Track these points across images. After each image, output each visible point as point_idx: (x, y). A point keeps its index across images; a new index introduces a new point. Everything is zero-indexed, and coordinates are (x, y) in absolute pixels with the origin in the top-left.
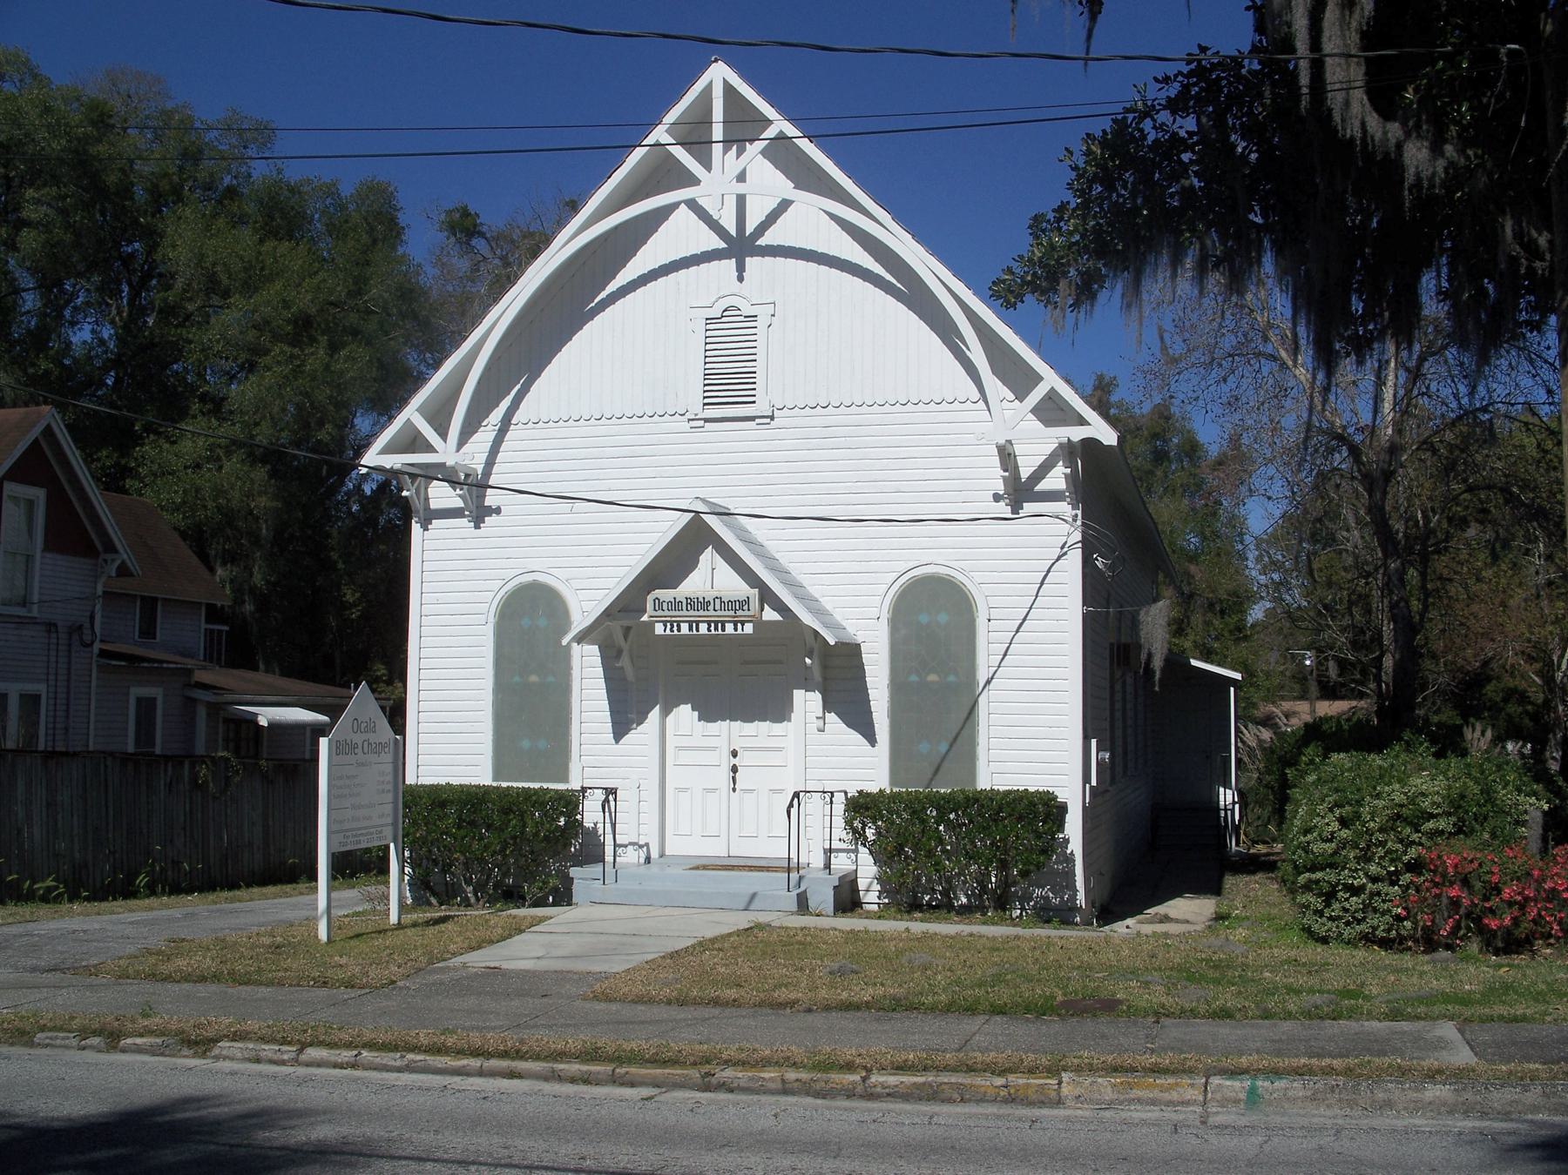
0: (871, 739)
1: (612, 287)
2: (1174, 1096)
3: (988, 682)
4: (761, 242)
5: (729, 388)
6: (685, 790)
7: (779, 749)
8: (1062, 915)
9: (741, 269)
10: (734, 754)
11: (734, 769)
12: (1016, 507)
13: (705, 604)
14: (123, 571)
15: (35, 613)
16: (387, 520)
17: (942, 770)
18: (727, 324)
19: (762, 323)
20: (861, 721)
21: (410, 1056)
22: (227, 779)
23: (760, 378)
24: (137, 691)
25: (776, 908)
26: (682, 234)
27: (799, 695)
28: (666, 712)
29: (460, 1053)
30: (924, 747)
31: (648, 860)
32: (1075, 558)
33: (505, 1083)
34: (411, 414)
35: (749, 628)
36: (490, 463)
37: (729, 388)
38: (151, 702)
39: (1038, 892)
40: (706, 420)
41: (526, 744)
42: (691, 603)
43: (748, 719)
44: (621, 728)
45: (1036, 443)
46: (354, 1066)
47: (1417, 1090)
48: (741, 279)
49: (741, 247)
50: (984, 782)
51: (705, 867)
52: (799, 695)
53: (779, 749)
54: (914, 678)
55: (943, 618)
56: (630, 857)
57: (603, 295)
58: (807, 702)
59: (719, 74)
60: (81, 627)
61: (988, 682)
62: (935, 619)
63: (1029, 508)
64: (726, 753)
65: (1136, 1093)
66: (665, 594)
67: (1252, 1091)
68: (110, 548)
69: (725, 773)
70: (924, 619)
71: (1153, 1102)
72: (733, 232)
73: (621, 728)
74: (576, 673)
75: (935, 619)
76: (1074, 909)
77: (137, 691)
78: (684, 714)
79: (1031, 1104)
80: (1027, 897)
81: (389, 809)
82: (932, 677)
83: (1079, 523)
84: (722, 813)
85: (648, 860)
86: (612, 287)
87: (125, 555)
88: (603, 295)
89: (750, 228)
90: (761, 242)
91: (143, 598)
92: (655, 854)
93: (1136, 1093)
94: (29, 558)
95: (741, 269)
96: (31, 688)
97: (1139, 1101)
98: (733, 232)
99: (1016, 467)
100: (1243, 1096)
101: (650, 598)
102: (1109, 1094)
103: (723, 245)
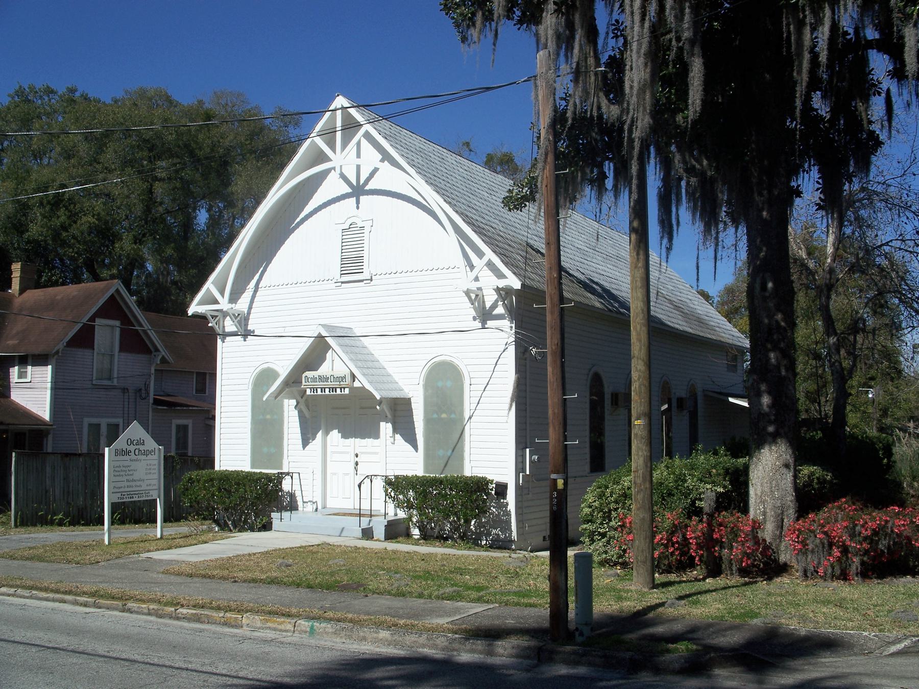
0: (416, 448)
1: (302, 215)
2: (282, 627)
3: (470, 418)
4: (367, 188)
5: (352, 266)
6: (335, 474)
7: (376, 453)
8: (502, 545)
9: (358, 202)
10: (357, 456)
11: (357, 464)
12: (484, 323)
13: (327, 379)
14: (164, 360)
15: (115, 382)
16: (203, 339)
17: (443, 465)
18: (352, 232)
19: (366, 230)
20: (411, 439)
21: (34, 592)
22: (173, 467)
23: (365, 260)
24: (176, 422)
25: (351, 537)
26: (332, 187)
27: (382, 424)
28: (327, 433)
29: (65, 593)
30: (441, 453)
31: (316, 510)
32: (512, 349)
33: (57, 605)
34: (209, 285)
35: (347, 391)
36: (250, 308)
37: (352, 266)
38: (185, 427)
39: (494, 531)
40: (342, 283)
41: (265, 450)
42: (321, 378)
43: (363, 437)
44: (305, 443)
45: (489, 285)
46: (13, 595)
47: (376, 633)
48: (358, 208)
49: (358, 191)
50: (468, 473)
51: (345, 514)
52: (382, 424)
53: (376, 453)
54: (435, 416)
55: (449, 384)
56: (310, 508)
57: (298, 220)
58: (386, 428)
59: (341, 101)
60: (140, 390)
61: (470, 418)
62: (445, 382)
63: (490, 323)
64: (353, 455)
65: (269, 624)
66: (309, 374)
67: (312, 627)
68: (157, 350)
69: (353, 465)
70: (440, 384)
71: (275, 629)
72: (355, 184)
73: (305, 443)
74: (286, 414)
75: (445, 382)
76: (512, 541)
77: (176, 422)
78: (335, 434)
79: (232, 627)
80: (489, 534)
81: (155, 482)
82: (444, 416)
83: (514, 331)
84: (340, 486)
85: (316, 510)
86: (302, 215)
87: (163, 352)
88: (298, 220)
89: (362, 182)
90: (367, 188)
91: (198, 373)
92: (320, 507)
93: (269, 624)
94: (112, 356)
95: (358, 202)
96: (94, 421)
97: (270, 628)
98: (355, 184)
99: (484, 302)
100: (308, 629)
101: (304, 375)
102: (259, 624)
103: (350, 191)
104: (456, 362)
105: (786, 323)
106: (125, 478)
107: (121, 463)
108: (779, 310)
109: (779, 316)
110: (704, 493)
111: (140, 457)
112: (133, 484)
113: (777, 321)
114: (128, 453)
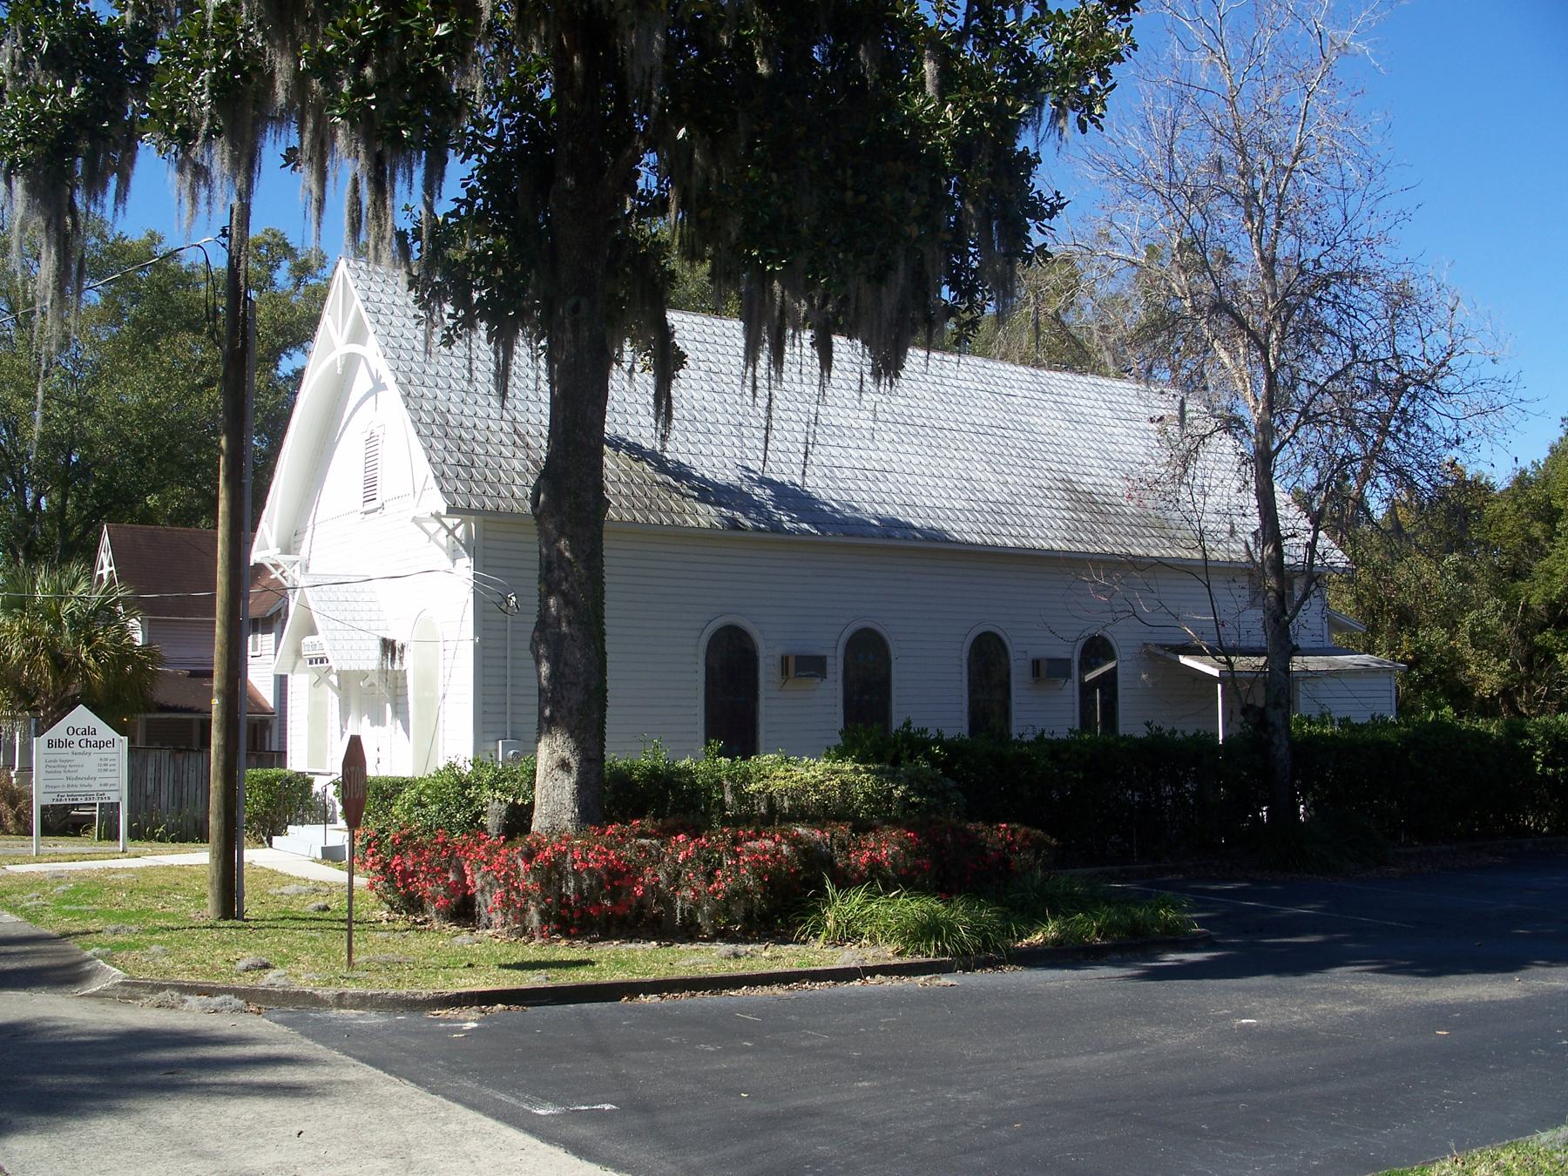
104: (883, 632)
105: (572, 552)
106: (63, 775)
107: (58, 757)
108: (562, 534)
109: (563, 543)
110: (487, 804)
111: (88, 750)
112: (78, 782)
113: (559, 551)
114: (69, 744)
